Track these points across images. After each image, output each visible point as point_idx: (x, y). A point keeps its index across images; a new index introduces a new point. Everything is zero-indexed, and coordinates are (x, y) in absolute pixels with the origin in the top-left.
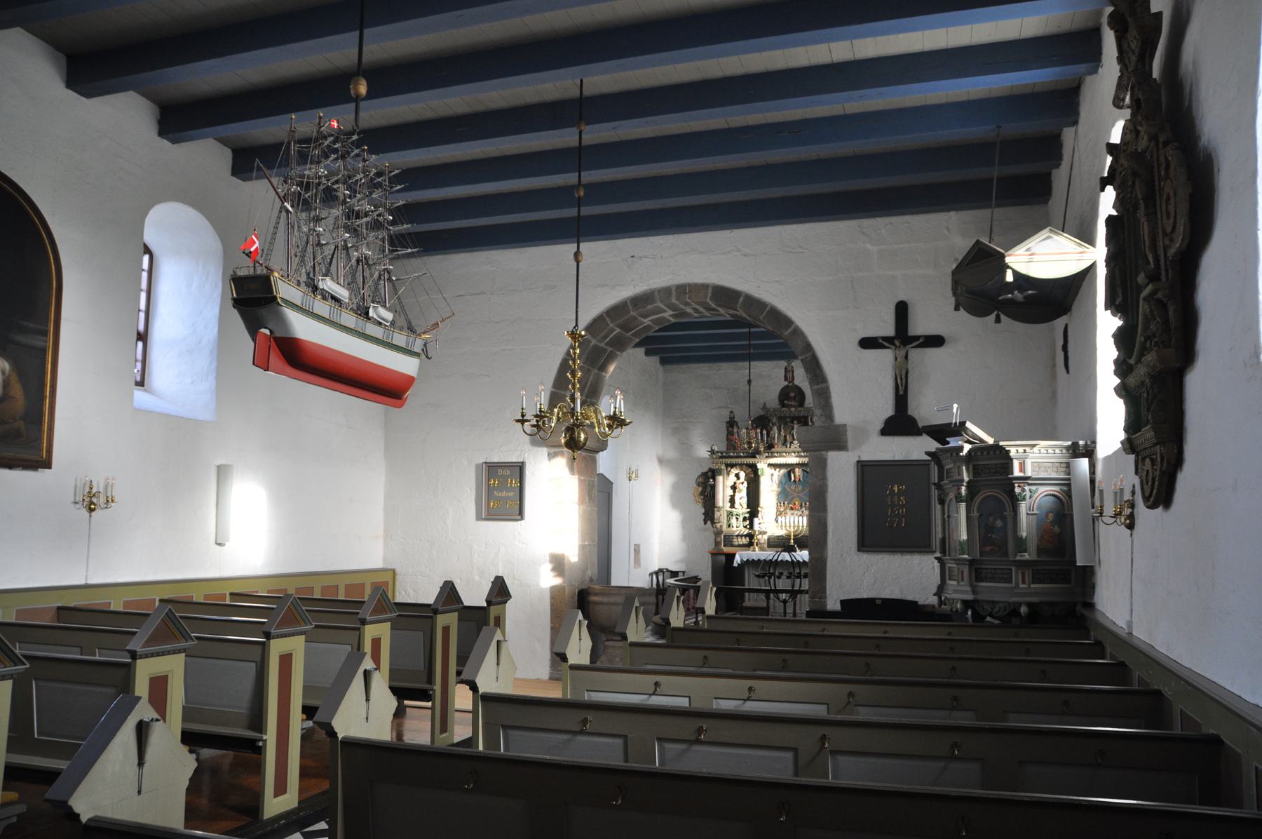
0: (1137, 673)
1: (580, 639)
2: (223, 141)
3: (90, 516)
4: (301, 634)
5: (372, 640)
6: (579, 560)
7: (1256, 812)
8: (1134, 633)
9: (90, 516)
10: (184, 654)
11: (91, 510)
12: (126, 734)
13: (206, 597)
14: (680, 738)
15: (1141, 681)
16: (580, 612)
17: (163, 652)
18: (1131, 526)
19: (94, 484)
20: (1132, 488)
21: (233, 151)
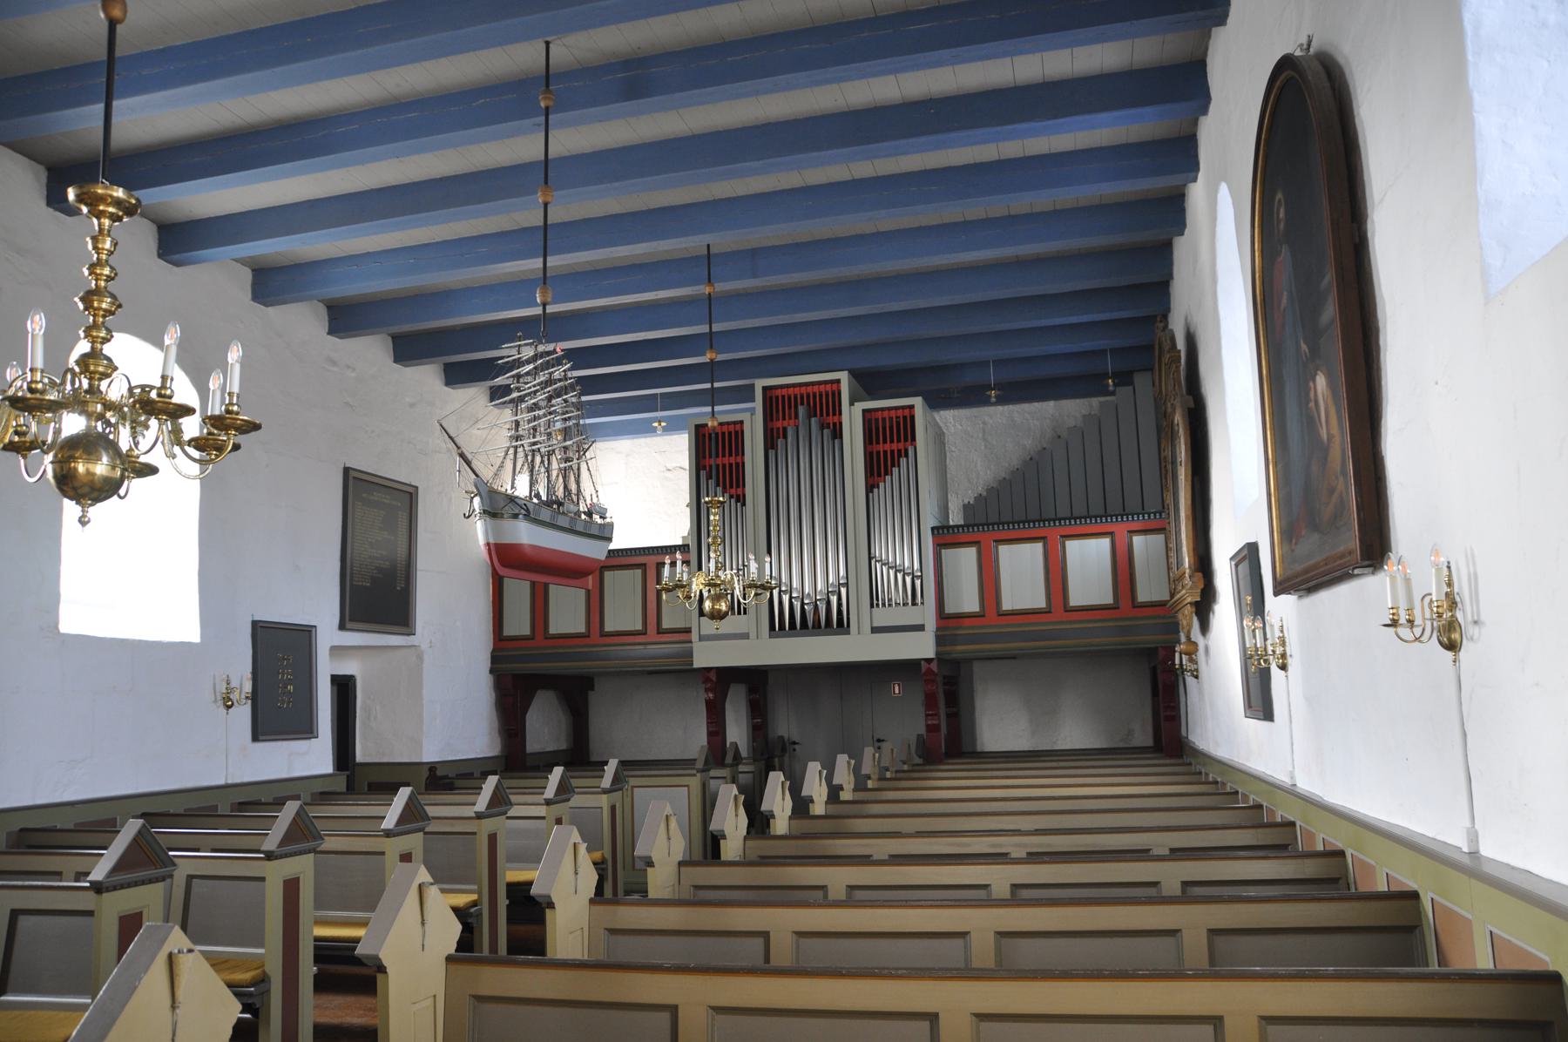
0: (1280, 813)
1: (669, 839)
2: (243, 261)
3: (227, 713)
4: (310, 853)
5: (284, 881)
6: (502, 751)
7: (1437, 968)
8: (1298, 785)
9: (227, 713)
10: (422, 833)
11: (229, 707)
12: (157, 972)
13: (185, 810)
14: (964, 818)
15: (1231, 788)
16: (668, 804)
17: (157, 879)
18: (1452, 646)
19: (231, 677)
20: (1210, 662)
21: (253, 271)
